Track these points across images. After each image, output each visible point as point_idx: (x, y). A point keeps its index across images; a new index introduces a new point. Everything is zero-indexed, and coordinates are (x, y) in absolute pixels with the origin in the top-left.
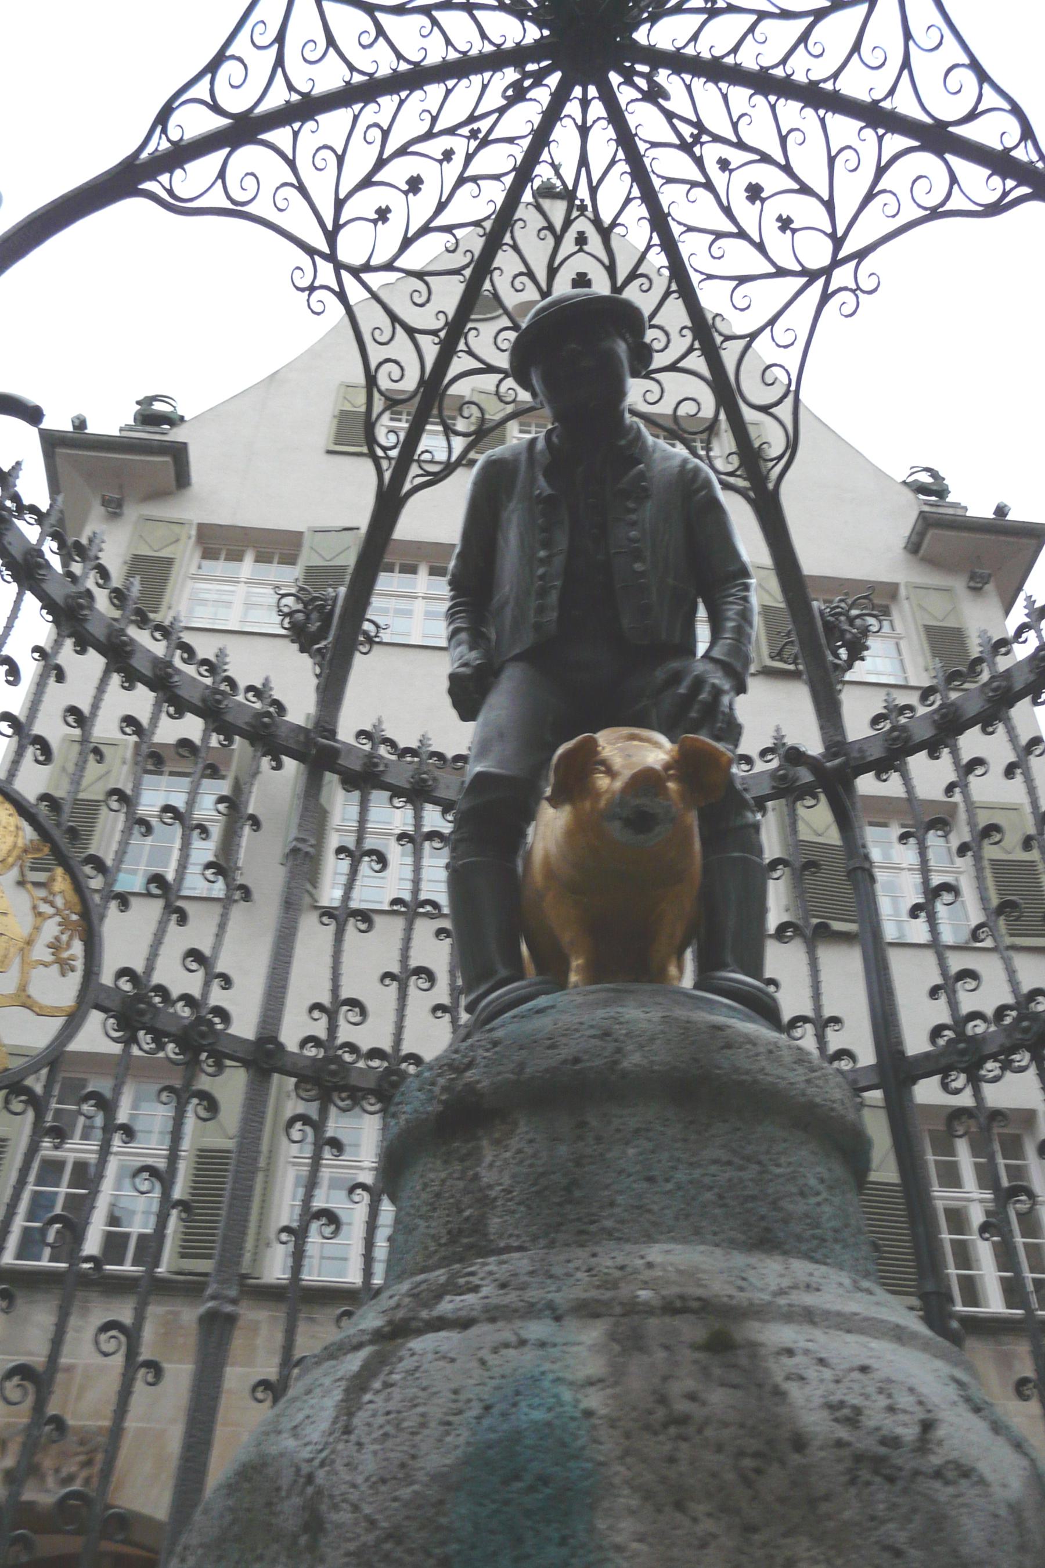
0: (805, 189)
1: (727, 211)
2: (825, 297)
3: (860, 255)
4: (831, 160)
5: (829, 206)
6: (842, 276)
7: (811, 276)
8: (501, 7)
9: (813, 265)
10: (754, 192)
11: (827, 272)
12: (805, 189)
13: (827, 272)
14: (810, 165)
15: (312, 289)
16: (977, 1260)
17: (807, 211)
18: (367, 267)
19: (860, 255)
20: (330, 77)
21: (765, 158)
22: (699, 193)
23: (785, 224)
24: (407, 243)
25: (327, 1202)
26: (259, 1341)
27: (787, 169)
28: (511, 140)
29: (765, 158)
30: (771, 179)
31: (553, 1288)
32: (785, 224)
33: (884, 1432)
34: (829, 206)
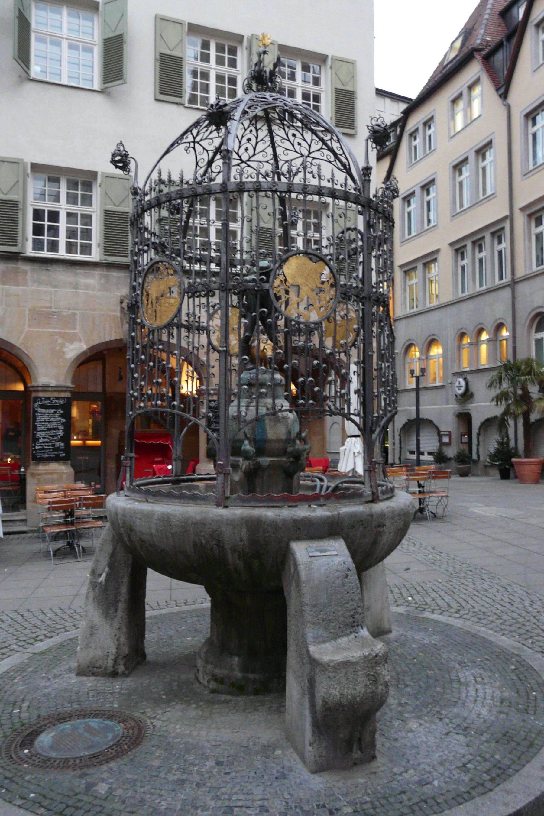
0: (255, 149)
1: (243, 137)
2: (238, 165)
3: (249, 166)
4: (263, 151)
5: (254, 155)
6: (243, 165)
7: (241, 160)
8: (406, 814)
9: (242, 158)
10: (249, 140)
11: (243, 162)
12: (255, 149)
13: (243, 162)
14: (260, 147)
15: (312, 164)
16: (156, 59)
17: (251, 152)
18: (309, 151)
19: (249, 166)
20: (270, 151)
21: (257, 138)
22: (244, 130)
23: (247, 149)
24: (305, 140)
25: (49, 195)
26: (28, 277)
27: (257, 143)
28: (312, 140)
29: (257, 138)
30: (253, 142)
31: (160, 712)
32: (247, 149)
33: (203, 664)
34: (254, 155)
